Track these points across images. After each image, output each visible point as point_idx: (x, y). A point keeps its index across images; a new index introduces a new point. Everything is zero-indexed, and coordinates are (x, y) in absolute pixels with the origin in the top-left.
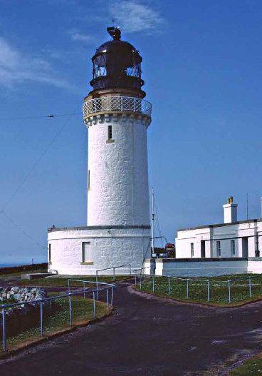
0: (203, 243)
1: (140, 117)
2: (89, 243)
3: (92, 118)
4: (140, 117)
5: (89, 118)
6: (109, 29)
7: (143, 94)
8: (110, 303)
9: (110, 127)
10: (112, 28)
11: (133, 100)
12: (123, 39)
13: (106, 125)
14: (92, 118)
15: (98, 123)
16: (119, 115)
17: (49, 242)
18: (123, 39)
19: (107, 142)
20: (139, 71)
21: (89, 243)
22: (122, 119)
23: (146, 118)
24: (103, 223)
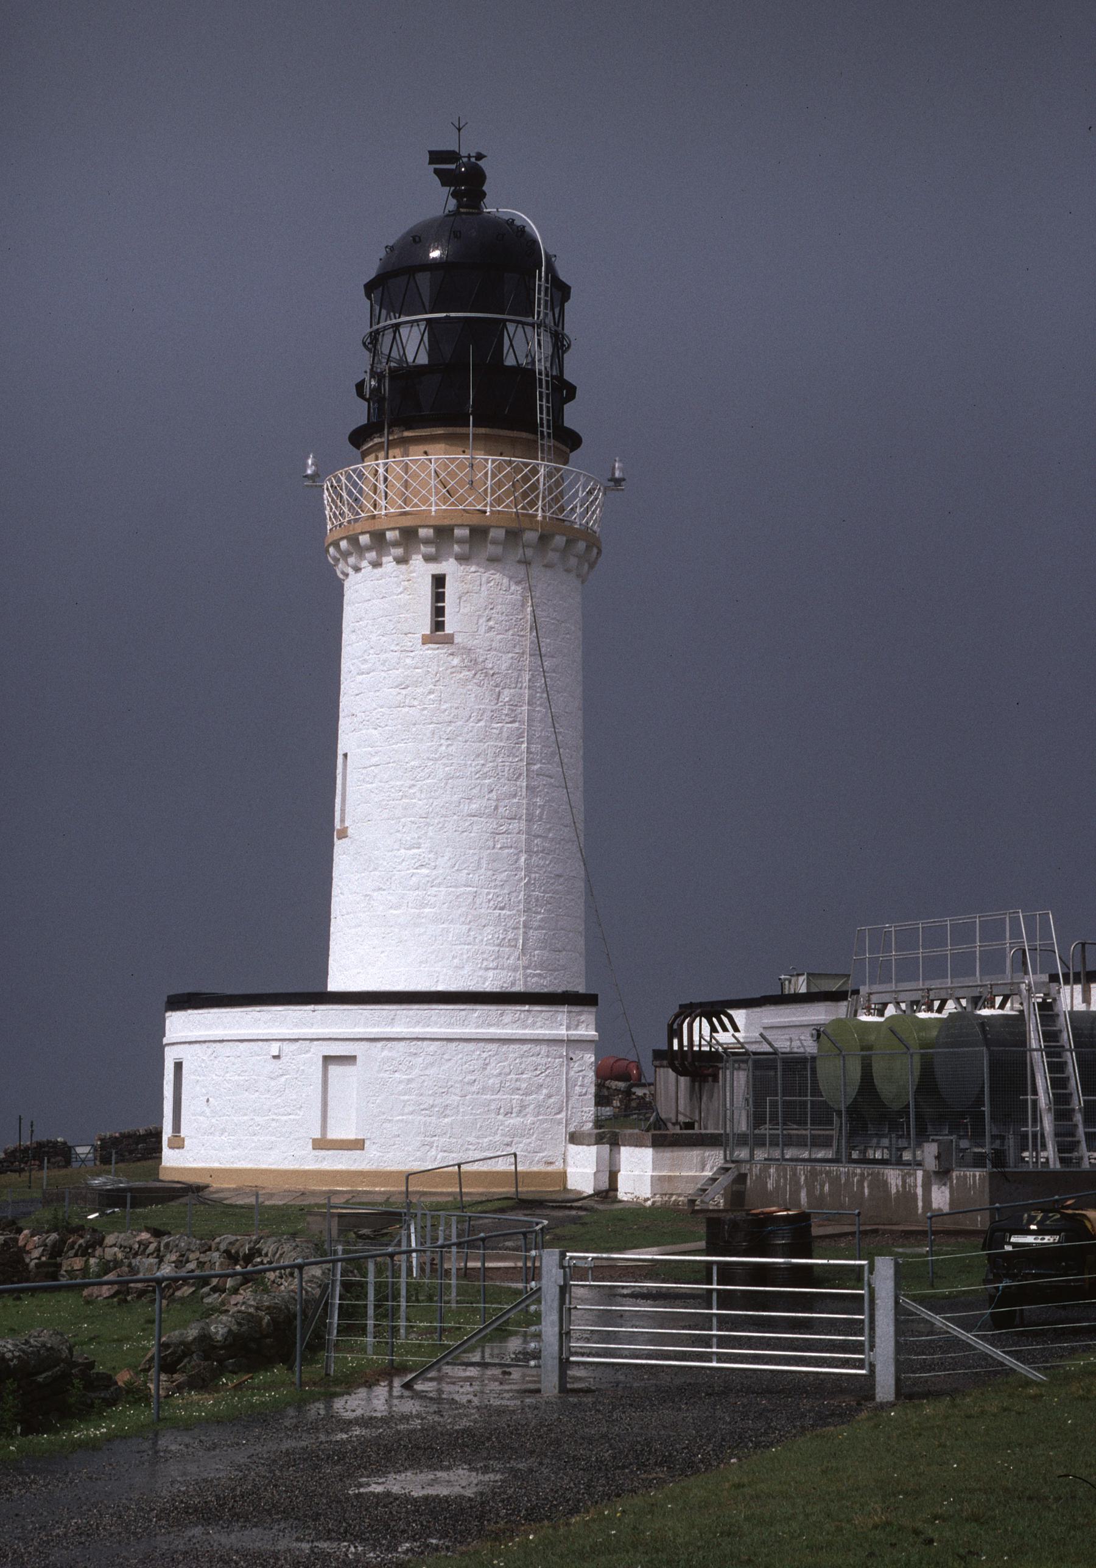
0: (538, 1391)
1: (559, 540)
2: (350, 1059)
3: (364, 539)
4: (559, 540)
5: (353, 540)
6: (436, 157)
7: (569, 440)
8: (975, 917)
9: (439, 581)
10: (451, 156)
11: (535, 471)
12: (496, 206)
13: (421, 570)
14: (364, 539)
15: (388, 561)
16: (479, 533)
17: (171, 1056)
18: (496, 206)
19: (426, 640)
20: (560, 344)
21: (350, 1059)
22: (491, 549)
23: (581, 545)
24: (489, 984)
